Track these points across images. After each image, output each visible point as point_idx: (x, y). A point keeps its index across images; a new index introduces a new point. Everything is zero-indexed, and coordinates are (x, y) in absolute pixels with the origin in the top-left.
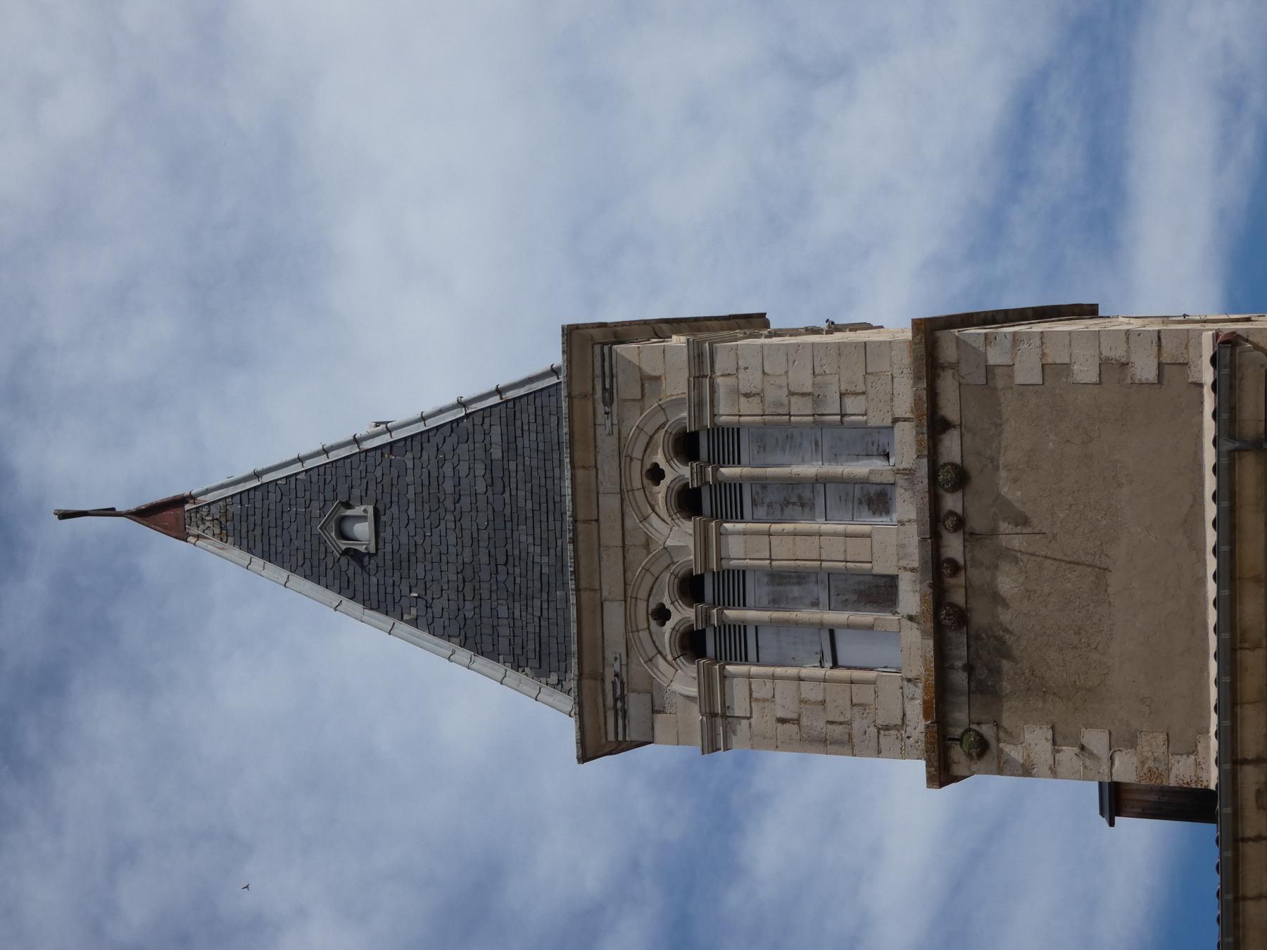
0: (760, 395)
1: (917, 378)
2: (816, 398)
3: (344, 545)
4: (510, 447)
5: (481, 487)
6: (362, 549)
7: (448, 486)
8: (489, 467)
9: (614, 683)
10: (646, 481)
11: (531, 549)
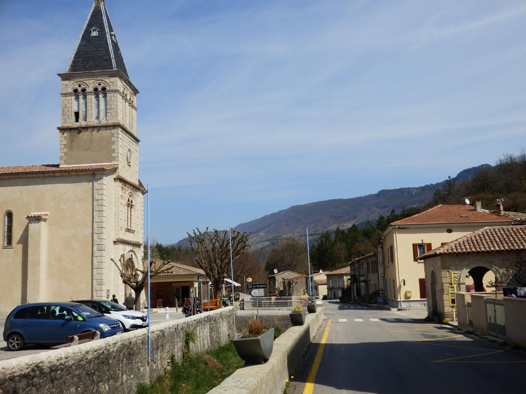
0: (111, 100)
1: (112, 123)
2: (110, 109)
3: (92, 31)
4: (105, 60)
5: (99, 55)
6: (91, 34)
7: (100, 49)
8: (102, 56)
9: (69, 79)
10: (98, 83)
11: (90, 64)
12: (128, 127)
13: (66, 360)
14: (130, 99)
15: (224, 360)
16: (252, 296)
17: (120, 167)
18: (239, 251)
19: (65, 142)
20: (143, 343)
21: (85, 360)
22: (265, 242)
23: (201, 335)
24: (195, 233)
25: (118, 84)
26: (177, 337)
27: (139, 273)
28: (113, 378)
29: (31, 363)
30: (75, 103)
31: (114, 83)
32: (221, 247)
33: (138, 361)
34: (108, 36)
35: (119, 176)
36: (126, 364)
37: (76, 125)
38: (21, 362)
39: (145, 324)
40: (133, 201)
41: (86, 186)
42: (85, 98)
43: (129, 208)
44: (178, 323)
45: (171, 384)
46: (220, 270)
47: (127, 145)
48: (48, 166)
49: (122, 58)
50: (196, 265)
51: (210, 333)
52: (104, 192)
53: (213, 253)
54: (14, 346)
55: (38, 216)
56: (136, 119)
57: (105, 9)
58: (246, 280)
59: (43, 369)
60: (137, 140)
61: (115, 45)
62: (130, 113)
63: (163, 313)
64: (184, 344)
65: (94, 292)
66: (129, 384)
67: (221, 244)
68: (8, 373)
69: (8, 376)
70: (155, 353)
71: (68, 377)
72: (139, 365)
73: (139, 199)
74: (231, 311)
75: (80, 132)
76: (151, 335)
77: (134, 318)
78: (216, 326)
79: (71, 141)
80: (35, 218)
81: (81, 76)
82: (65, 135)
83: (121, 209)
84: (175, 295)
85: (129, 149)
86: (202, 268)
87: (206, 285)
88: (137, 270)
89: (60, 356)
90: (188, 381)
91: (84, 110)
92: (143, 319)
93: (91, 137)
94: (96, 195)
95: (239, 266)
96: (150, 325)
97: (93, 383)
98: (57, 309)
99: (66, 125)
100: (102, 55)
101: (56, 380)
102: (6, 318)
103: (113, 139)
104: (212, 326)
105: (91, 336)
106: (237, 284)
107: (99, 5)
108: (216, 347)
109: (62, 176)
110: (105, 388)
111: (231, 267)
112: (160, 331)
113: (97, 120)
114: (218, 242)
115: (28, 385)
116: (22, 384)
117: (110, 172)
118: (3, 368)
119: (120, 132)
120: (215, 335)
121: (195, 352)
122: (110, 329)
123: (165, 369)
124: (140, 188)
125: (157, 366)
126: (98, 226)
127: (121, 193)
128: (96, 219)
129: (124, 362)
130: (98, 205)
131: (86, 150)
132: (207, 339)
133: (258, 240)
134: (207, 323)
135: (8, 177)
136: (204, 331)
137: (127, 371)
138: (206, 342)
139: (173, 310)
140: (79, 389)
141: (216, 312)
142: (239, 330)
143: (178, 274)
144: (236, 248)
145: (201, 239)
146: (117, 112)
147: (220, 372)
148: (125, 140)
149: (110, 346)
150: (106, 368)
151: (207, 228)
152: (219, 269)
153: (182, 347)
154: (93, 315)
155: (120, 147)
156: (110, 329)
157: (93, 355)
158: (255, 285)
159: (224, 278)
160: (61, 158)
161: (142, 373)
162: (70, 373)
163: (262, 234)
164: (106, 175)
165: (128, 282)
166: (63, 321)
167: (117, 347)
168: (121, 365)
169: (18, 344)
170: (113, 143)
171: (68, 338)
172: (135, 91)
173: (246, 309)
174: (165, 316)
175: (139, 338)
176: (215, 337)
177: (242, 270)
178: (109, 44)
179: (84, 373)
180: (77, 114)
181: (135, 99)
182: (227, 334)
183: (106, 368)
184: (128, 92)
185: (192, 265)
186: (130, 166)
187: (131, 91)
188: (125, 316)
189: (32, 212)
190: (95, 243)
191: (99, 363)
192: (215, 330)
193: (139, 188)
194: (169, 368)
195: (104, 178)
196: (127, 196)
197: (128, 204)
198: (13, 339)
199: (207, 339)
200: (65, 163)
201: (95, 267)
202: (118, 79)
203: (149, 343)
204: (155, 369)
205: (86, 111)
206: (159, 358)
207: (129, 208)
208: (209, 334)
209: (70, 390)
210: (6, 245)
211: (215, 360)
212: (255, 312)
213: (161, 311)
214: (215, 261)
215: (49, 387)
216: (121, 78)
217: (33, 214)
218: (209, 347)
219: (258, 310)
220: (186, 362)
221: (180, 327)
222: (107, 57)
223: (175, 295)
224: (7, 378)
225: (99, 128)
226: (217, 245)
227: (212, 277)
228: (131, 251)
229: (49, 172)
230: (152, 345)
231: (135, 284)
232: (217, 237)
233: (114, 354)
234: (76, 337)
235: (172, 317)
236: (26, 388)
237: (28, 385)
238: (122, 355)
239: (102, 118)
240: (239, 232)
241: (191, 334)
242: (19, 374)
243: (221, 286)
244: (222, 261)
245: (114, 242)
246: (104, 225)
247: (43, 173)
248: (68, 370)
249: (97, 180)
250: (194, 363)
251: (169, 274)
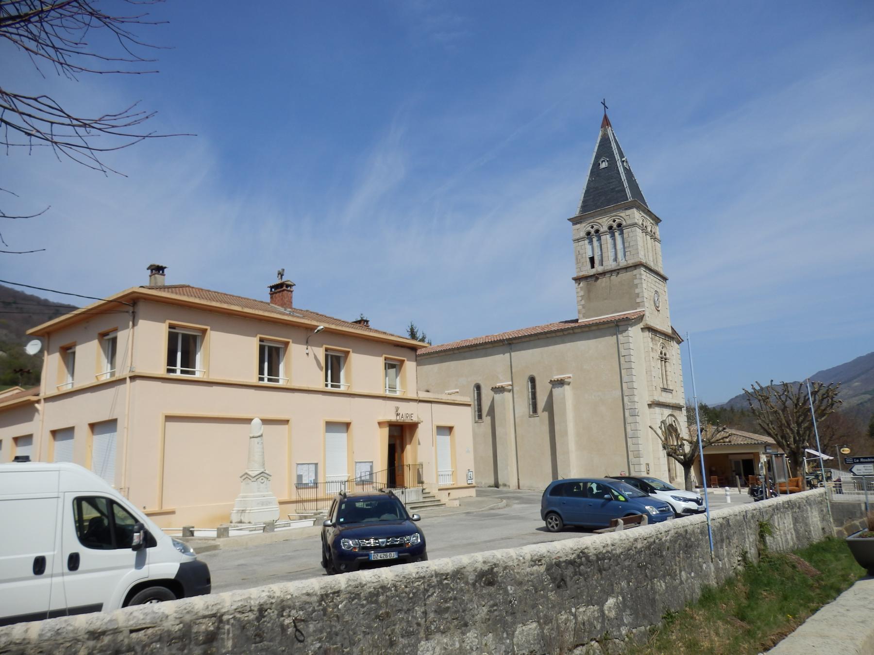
0: (629, 237)
2: (629, 247)
3: (601, 163)
5: (611, 187)
7: (611, 181)
12: (652, 265)
13: (613, 547)
14: (651, 231)
15: (820, 564)
16: (854, 474)
17: (647, 314)
18: (825, 410)
19: (582, 293)
20: (702, 533)
21: (634, 549)
22: (862, 396)
23: (781, 526)
24: (754, 389)
25: (636, 215)
26: (747, 528)
27: (685, 442)
28: (670, 575)
29: (576, 548)
30: (589, 247)
32: (796, 405)
33: (699, 556)
34: (619, 164)
35: (647, 324)
36: (683, 559)
37: (592, 272)
38: (565, 546)
39: (701, 508)
40: (667, 353)
41: (611, 340)
42: (599, 239)
43: (663, 362)
44: (747, 509)
45: (746, 589)
46: (797, 438)
47: (653, 286)
48: (566, 322)
49: (637, 184)
50: (758, 431)
51: (794, 524)
52: (632, 346)
53: (784, 414)
54: (553, 527)
55: (561, 380)
56: (660, 253)
57: (613, 134)
58: (840, 451)
59: (589, 557)
60: (665, 279)
61: (628, 172)
62: (652, 247)
63: (722, 495)
64: (758, 538)
65: (632, 467)
66: (690, 584)
67: (795, 402)
68: (554, 557)
69: (554, 561)
70: (719, 547)
71: (617, 568)
72: (700, 560)
73: (674, 350)
74: (823, 495)
75: (597, 279)
76: (712, 523)
77: (686, 500)
78: (802, 516)
79: (589, 291)
81: (593, 217)
82: (581, 285)
83: (653, 364)
84: (734, 471)
85: (656, 291)
86: (769, 435)
87: (780, 459)
88: (683, 439)
89: (605, 543)
90: (771, 589)
91: (600, 253)
92: (697, 501)
93: (610, 283)
94: (622, 350)
95: (826, 431)
96: (709, 509)
97: (646, 578)
98: (594, 486)
99: (581, 274)
100: (614, 186)
101: (605, 570)
102: (542, 495)
103: (636, 282)
104: (795, 515)
105: (638, 521)
106: (825, 457)
108: (806, 544)
109: (583, 332)
110: (661, 586)
111: (814, 433)
112: (723, 518)
113: (615, 263)
114: (790, 398)
115: (575, 573)
116: (569, 572)
117: (635, 322)
118: (548, 552)
119: (643, 272)
120: (801, 528)
121: (775, 550)
122: (658, 512)
123: (735, 569)
124: (674, 336)
125: (724, 564)
127: (651, 345)
128: (625, 379)
129: (681, 555)
131: (606, 299)
132: (791, 533)
133: (851, 392)
134: (788, 511)
135: (528, 339)
136: (785, 522)
137: (686, 567)
138: (789, 537)
139: (735, 491)
140: (631, 584)
141: (799, 496)
142: (839, 522)
143: (736, 443)
144: (819, 406)
145: (764, 396)
146: (637, 249)
147: (817, 581)
148: (650, 280)
149: (661, 534)
150: (659, 562)
151: (772, 381)
152: (796, 436)
153: (756, 541)
154: (635, 495)
155: (644, 290)
156: (658, 512)
157: (642, 543)
158: (857, 458)
159: (804, 448)
160: (579, 312)
161: (704, 571)
162: (618, 564)
163: (856, 384)
164: (632, 325)
165: (673, 454)
166: (603, 501)
167: (670, 535)
168: (677, 558)
169: (557, 525)
170: (636, 286)
171: (612, 522)
172: (657, 220)
173: (845, 493)
174: (726, 498)
175: (697, 526)
176: (802, 530)
177: (831, 437)
178: (621, 172)
179: (634, 564)
180: (592, 260)
181: (657, 230)
182: (820, 527)
183: (659, 562)
184: (649, 222)
185: (753, 430)
186: (658, 311)
187: (652, 221)
188: (675, 497)
190: (626, 407)
191: (650, 555)
192: (801, 520)
193: (673, 337)
194: (739, 568)
195: (630, 329)
196: (659, 348)
197: (662, 358)
198: (552, 519)
199: (791, 533)
200: (584, 317)
201: (629, 435)
202: (635, 210)
203: (711, 534)
204: (722, 568)
205: (602, 254)
206: (725, 554)
207: (663, 362)
208: (792, 526)
209: (621, 584)
210: (531, 413)
211: (807, 563)
212: (862, 498)
213: (718, 491)
214: (789, 425)
215: (597, 578)
216: (638, 208)
217: (499, 385)
218: (794, 544)
219: (866, 494)
220: (764, 562)
221: (749, 515)
222: (620, 188)
223: (734, 471)
224: (554, 563)
225: (617, 271)
226: (789, 403)
227: (786, 447)
228: (671, 415)
229: (568, 329)
230: (715, 535)
231: (682, 457)
232: (788, 392)
233: (667, 544)
234: (621, 521)
235: (735, 500)
236: (574, 576)
237: (575, 573)
238: (677, 546)
239: (620, 259)
240: (822, 384)
241: (766, 524)
242: (564, 559)
243: (801, 460)
244: (799, 425)
245: (648, 405)
246: (635, 385)
247: (562, 330)
248: (617, 560)
249: (622, 332)
250: (776, 564)
251: (726, 444)
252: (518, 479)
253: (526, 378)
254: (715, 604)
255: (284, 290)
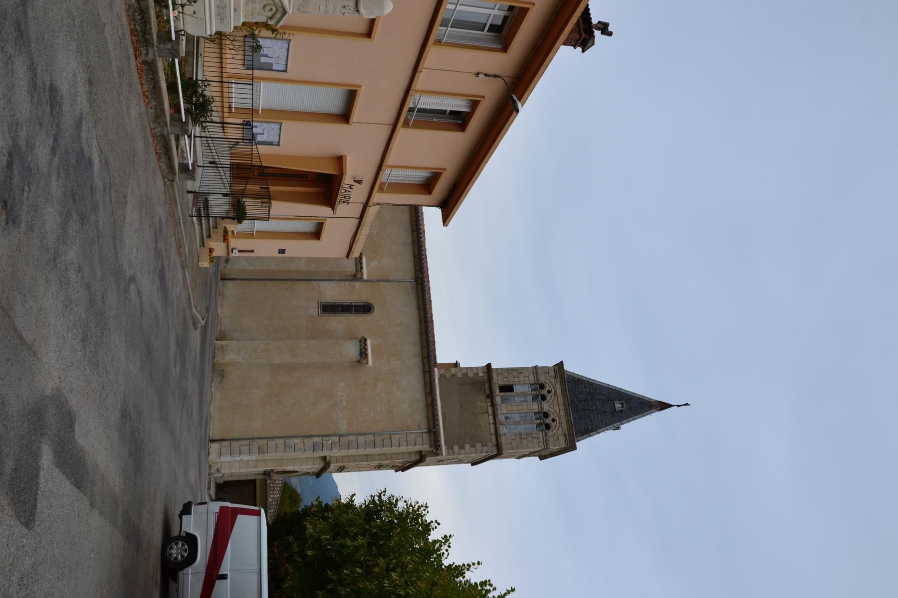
0: (533, 438)
1: (501, 443)
3: (621, 402)
31: (558, 441)
65: (247, 442)
75: (488, 397)
80: (364, 350)
99: (494, 375)
103: (479, 445)
107: (653, 408)
126: (351, 441)
130: (383, 440)
170: (473, 446)
186: (479, 563)
189: (371, 341)
245: (325, 457)
252: (234, 279)
253: (371, 300)
254: (78, 92)
255: (580, 35)
